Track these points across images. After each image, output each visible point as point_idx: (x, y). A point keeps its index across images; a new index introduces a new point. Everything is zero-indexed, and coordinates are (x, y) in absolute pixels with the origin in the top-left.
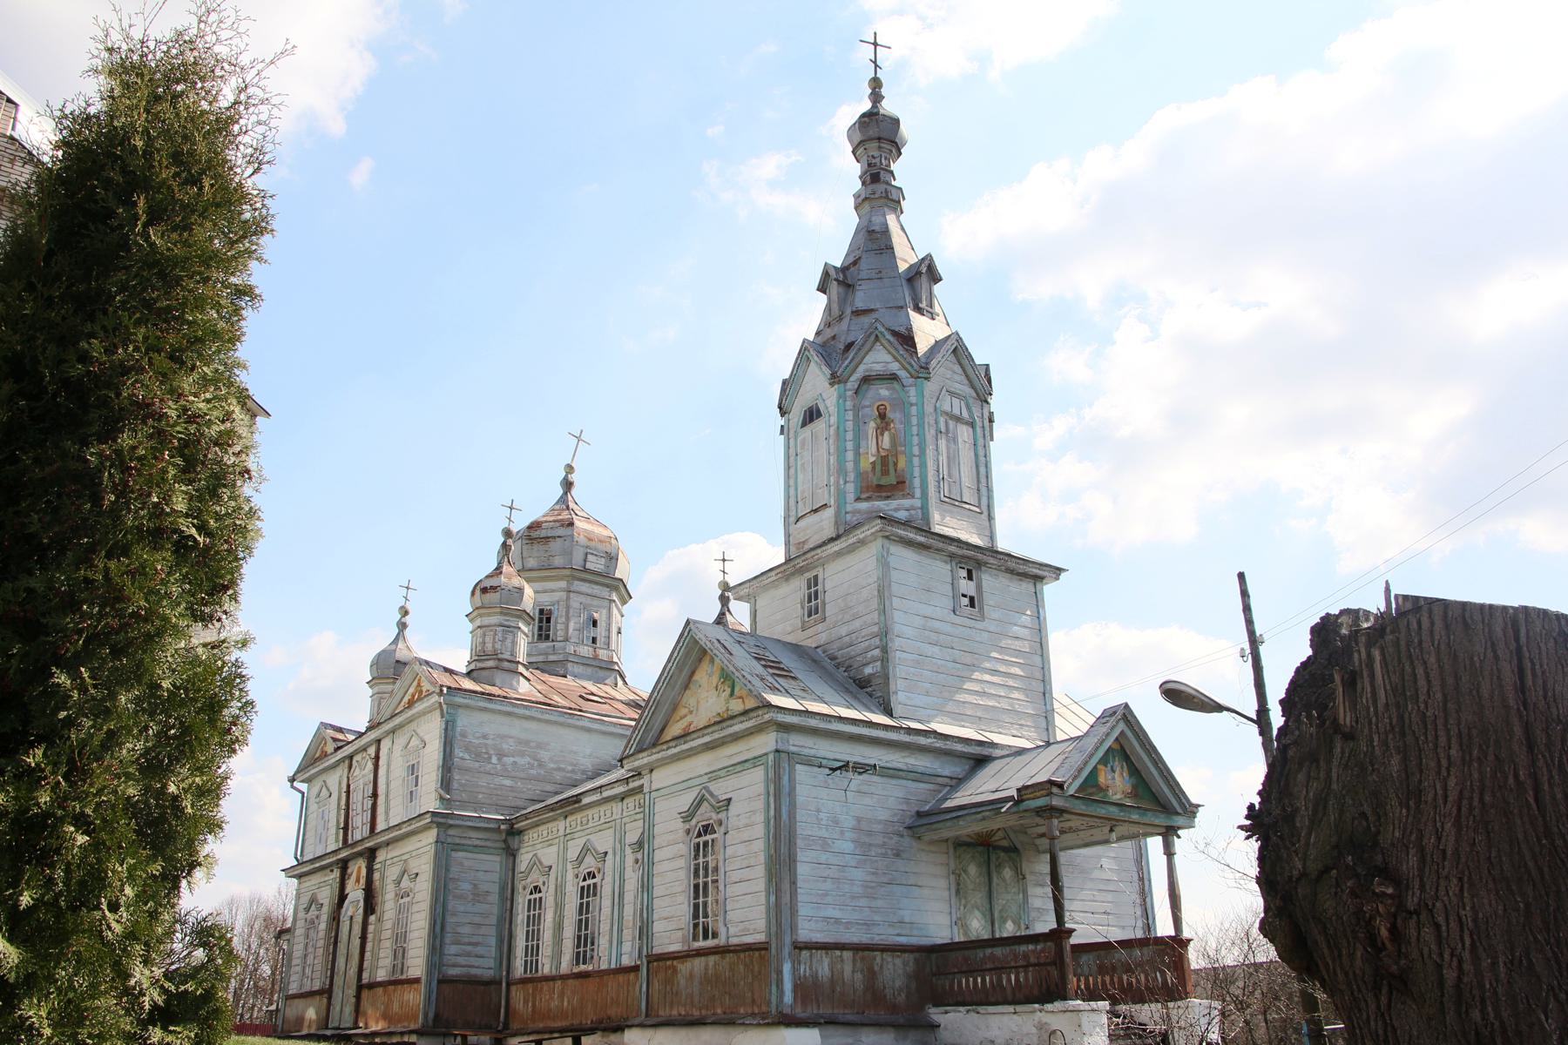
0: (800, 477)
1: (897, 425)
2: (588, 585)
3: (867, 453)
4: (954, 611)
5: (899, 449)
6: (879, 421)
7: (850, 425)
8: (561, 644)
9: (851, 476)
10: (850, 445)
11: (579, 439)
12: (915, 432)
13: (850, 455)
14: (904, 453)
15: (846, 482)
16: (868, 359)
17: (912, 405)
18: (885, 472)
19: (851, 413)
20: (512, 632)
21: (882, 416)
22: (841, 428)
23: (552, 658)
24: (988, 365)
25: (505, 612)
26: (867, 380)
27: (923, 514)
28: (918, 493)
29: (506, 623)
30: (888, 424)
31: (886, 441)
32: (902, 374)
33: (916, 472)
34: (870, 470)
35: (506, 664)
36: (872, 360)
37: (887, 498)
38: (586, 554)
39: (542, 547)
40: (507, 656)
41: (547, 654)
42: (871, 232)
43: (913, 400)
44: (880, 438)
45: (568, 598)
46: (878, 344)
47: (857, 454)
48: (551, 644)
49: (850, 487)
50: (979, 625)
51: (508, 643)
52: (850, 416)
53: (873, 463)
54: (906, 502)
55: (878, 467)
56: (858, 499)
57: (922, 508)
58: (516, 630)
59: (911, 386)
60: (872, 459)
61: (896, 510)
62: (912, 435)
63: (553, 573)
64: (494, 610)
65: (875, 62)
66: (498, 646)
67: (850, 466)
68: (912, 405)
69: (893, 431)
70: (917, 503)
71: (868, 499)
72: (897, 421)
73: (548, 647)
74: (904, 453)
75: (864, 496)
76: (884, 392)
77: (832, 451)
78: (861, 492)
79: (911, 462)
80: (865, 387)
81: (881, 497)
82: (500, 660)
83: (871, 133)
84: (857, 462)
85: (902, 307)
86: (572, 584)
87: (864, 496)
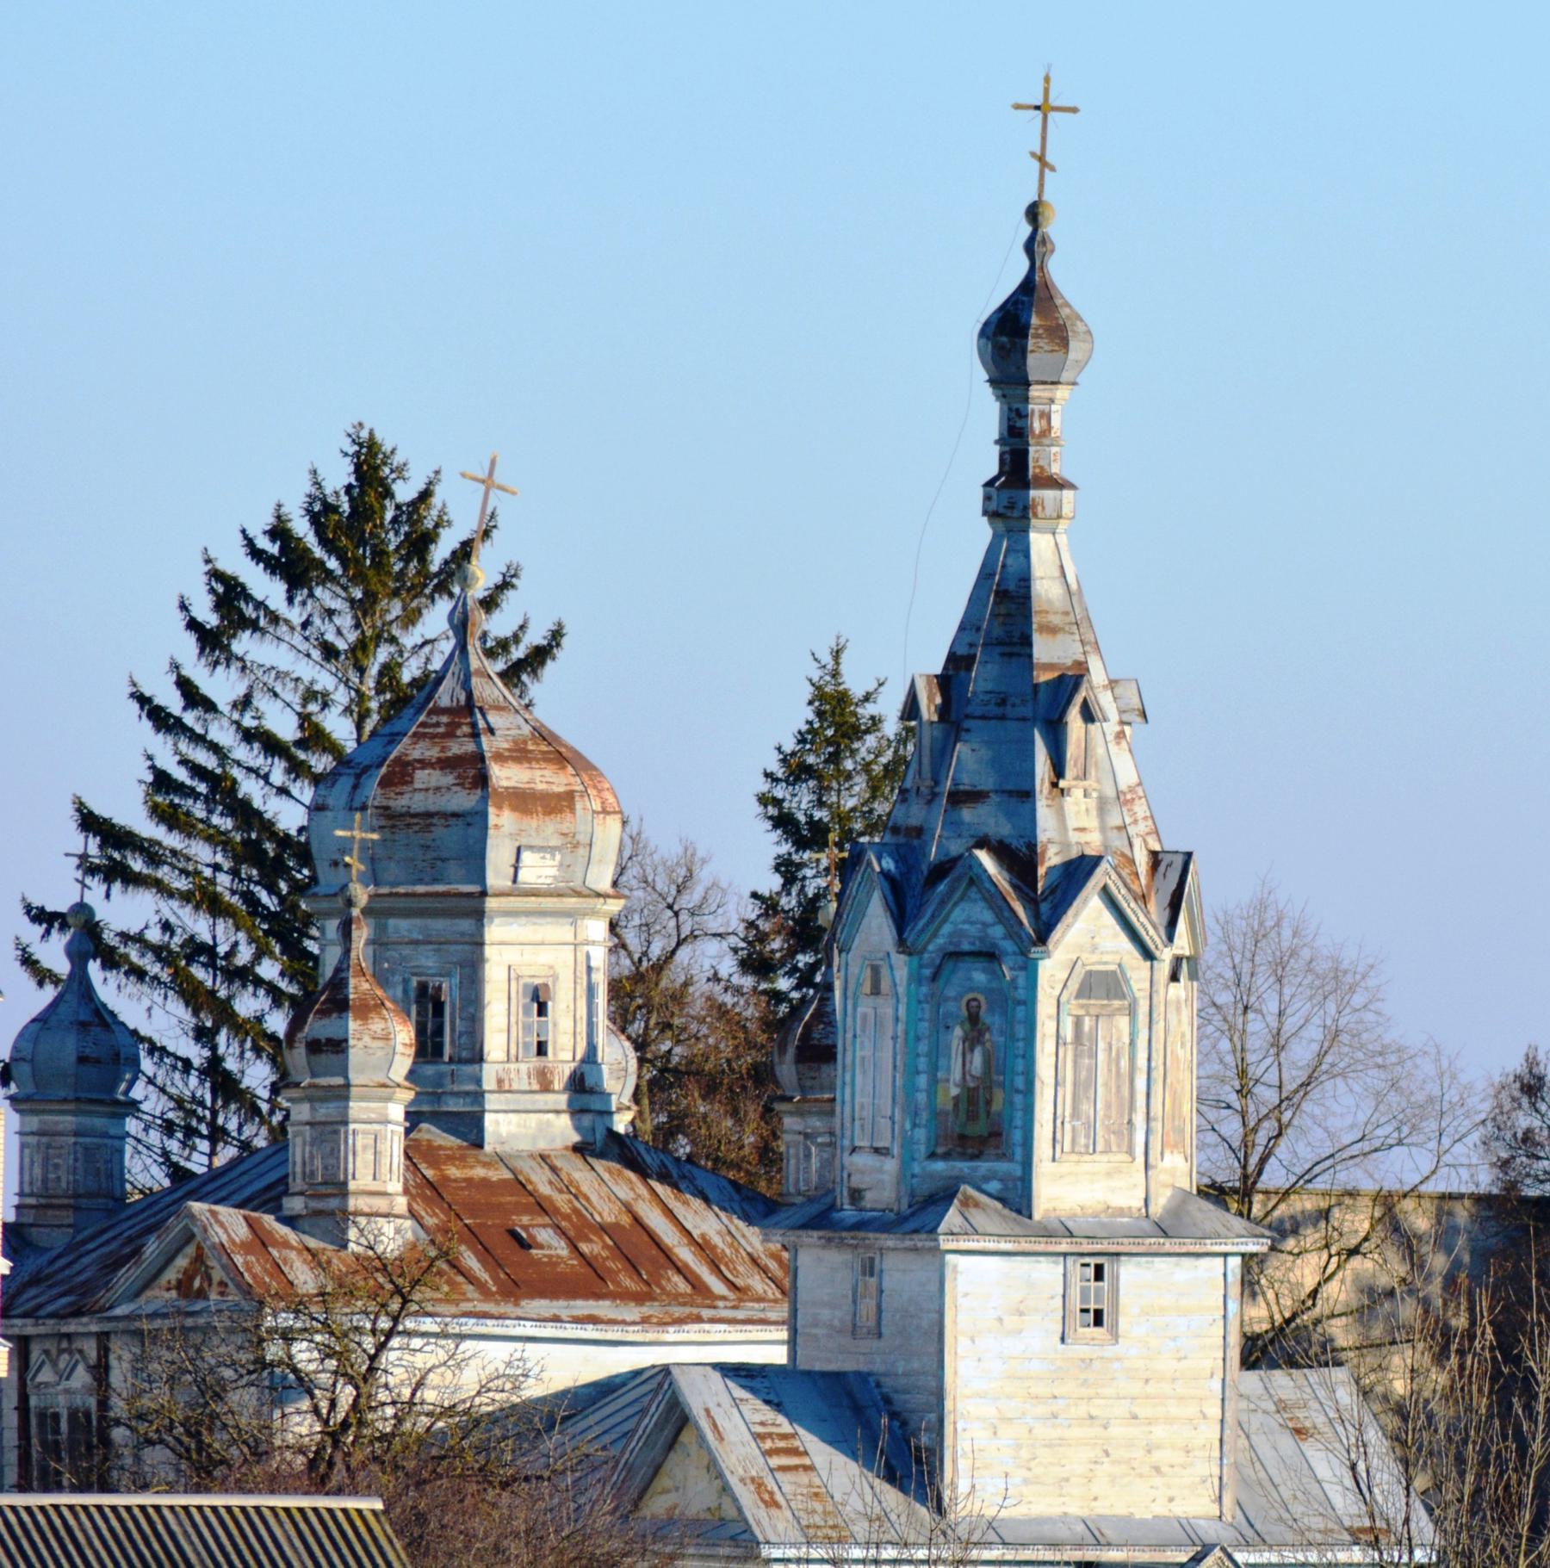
0: (859, 1079)
1: (994, 1038)
3: (948, 1081)
6: (967, 1026)
10: (922, 1063)
13: (922, 1081)
14: (1002, 1085)
15: (914, 1125)
18: (972, 1116)
21: (973, 1018)
26: (954, 956)
28: (1018, 1152)
30: (981, 1034)
34: (950, 1107)
37: (975, 1157)
42: (1002, 595)
44: (968, 1057)
46: (974, 889)
47: (934, 1081)
49: (921, 1134)
53: (957, 1099)
54: (1002, 1167)
55: (963, 1106)
56: (932, 1156)
60: (955, 1091)
65: (1041, 159)
67: (922, 1097)
69: (988, 1045)
71: (946, 1156)
76: (980, 977)
77: (898, 1063)
78: (937, 1145)
79: (1011, 1103)
80: (949, 965)
84: (932, 1092)
87: (940, 1150)
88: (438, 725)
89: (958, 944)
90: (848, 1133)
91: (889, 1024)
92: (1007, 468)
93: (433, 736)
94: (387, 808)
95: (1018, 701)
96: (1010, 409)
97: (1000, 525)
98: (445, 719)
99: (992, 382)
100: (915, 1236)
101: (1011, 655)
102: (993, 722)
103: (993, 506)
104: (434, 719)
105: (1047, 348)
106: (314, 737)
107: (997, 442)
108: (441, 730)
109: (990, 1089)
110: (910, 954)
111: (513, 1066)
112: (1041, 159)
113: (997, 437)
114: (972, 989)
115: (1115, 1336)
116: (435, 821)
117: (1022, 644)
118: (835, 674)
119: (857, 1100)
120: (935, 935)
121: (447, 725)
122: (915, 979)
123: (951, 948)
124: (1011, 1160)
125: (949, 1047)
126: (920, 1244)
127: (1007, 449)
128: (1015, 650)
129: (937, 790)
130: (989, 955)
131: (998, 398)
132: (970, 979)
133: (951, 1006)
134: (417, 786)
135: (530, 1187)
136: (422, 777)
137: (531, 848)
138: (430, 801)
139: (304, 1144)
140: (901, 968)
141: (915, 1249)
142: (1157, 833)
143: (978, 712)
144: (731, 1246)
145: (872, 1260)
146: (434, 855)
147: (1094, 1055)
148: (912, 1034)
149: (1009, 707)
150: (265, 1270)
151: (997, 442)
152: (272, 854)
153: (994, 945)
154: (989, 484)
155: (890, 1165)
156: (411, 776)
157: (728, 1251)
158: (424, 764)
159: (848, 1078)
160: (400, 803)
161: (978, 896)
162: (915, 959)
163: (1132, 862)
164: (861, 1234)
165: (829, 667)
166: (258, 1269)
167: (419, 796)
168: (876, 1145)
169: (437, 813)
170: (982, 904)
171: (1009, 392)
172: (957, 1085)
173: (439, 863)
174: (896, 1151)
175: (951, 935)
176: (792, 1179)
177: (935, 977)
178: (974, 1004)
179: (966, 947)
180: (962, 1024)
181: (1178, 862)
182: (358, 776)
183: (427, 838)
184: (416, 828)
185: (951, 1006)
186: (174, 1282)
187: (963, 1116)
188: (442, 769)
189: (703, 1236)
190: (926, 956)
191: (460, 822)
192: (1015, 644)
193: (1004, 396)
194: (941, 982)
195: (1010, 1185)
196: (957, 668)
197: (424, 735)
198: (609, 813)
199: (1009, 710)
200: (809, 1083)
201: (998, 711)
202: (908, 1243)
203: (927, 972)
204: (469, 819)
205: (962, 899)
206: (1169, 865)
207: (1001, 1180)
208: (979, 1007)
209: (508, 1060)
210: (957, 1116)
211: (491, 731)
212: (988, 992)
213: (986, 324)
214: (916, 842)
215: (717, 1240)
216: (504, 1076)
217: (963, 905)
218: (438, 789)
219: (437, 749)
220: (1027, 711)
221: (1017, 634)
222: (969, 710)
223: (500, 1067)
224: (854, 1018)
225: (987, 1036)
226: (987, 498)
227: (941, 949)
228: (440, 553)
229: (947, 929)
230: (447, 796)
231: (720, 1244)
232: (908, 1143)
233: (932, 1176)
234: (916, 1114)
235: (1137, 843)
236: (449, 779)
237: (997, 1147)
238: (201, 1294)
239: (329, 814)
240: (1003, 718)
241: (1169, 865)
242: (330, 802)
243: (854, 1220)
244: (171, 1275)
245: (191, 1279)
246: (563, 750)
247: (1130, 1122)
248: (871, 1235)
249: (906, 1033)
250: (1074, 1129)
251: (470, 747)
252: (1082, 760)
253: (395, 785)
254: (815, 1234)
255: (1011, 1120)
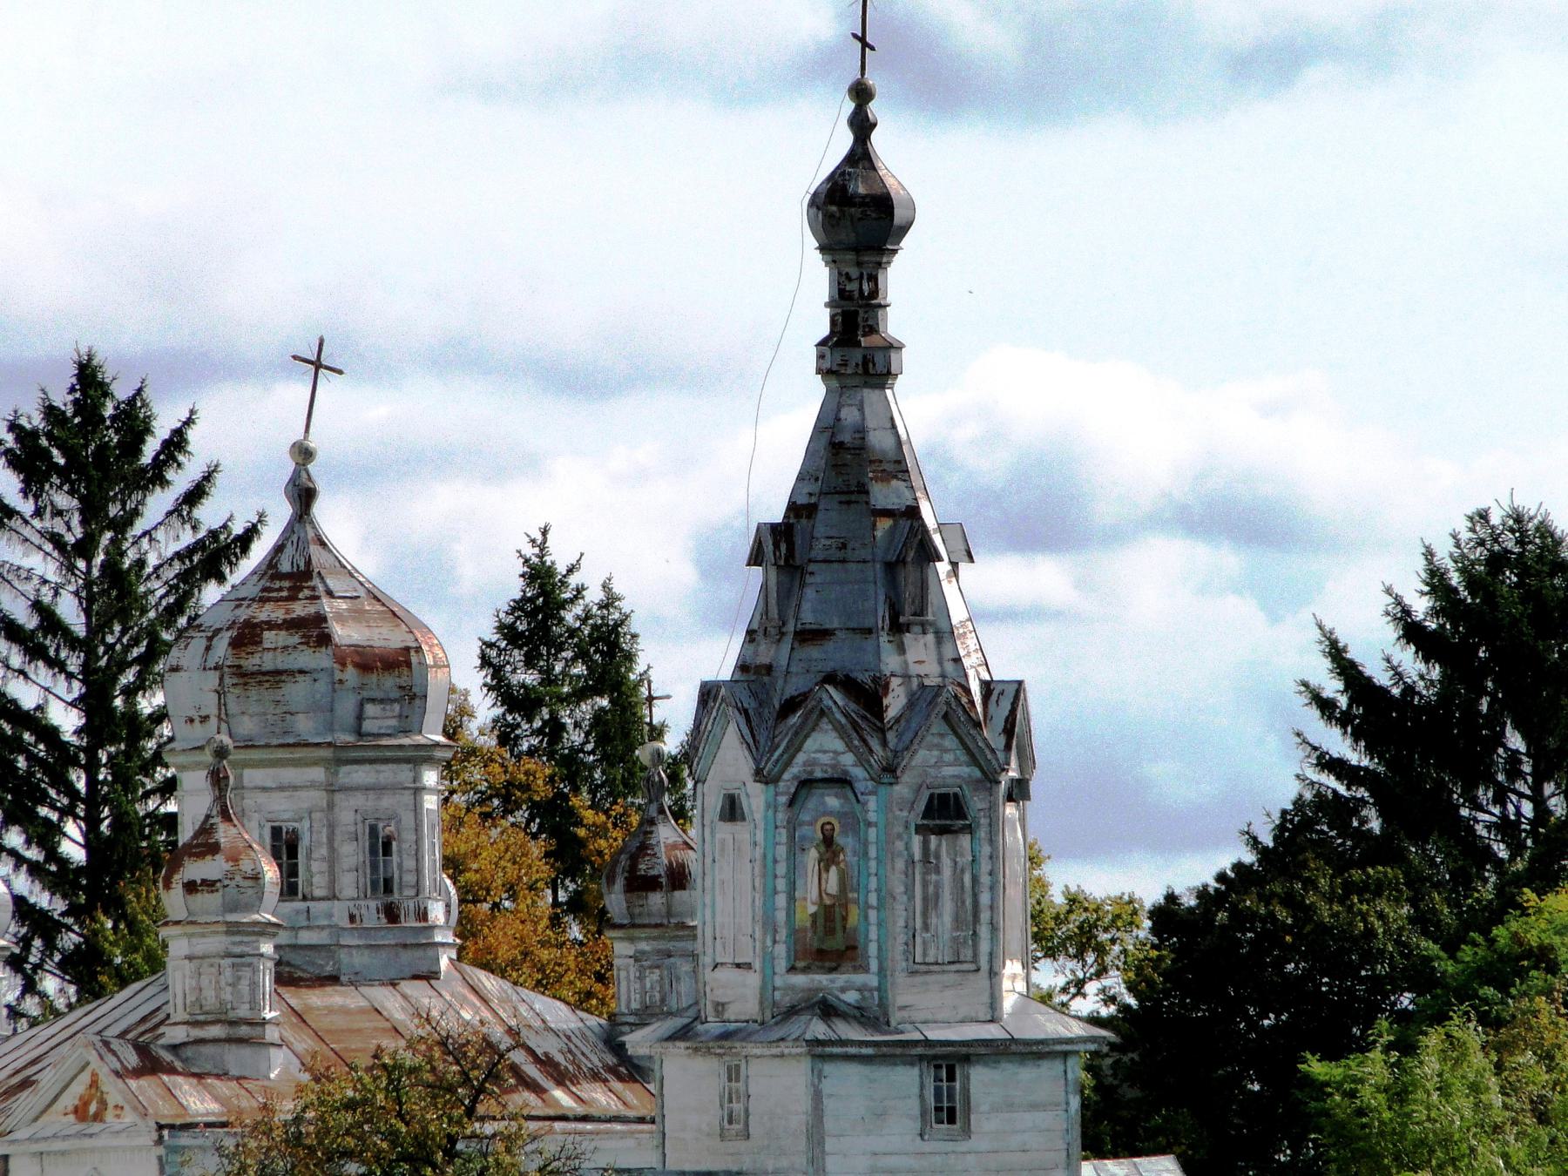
0: (719, 899)
1: (848, 857)
2: (367, 767)
3: (805, 899)
4: (921, 1135)
5: (850, 895)
6: (822, 849)
7: (782, 851)
8: (323, 905)
9: (782, 934)
10: (781, 884)
11: (318, 365)
12: (873, 870)
13: (781, 900)
14: (856, 902)
15: (775, 942)
16: (810, 744)
17: (869, 824)
18: (830, 931)
19: (784, 832)
20: (250, 965)
21: (828, 841)
22: (770, 857)
23: (306, 938)
24: (1020, 683)
25: (234, 929)
26: (807, 784)
27: (880, 999)
28: (874, 965)
29: (237, 950)
30: (835, 854)
31: (832, 882)
32: (858, 772)
33: (873, 935)
34: (808, 924)
35: (244, 1031)
36: (816, 747)
37: (832, 970)
38: (361, 705)
39: (269, 695)
40: (243, 1012)
41: (295, 929)
42: (836, 447)
43: (872, 817)
44: (824, 876)
45: (331, 806)
46: (825, 720)
47: (791, 898)
48: (302, 905)
49: (781, 950)
50: (963, 1146)
51: (244, 986)
52: (783, 836)
53: (814, 916)
54: (859, 979)
55: (821, 921)
56: (792, 969)
57: (879, 989)
58: (254, 960)
59: (871, 793)
60: (812, 909)
61: (843, 990)
62: (869, 875)
63: (299, 754)
64: (213, 928)
65: (862, 39)
66: (227, 995)
67: (781, 916)
68: (869, 824)
69: (842, 865)
70: (873, 980)
71: (806, 970)
72: (848, 851)
73: (298, 912)
74: (856, 902)
75: (800, 964)
76: (833, 802)
77: (757, 885)
78: (796, 959)
79: (866, 917)
80: (804, 792)
81: (822, 968)
82: (233, 1023)
83: (843, 236)
84: (791, 912)
85: (869, 631)
86: (336, 773)
87: (800, 964)
88: (281, 589)
89: (811, 773)
90: (709, 951)
91: (747, 848)
92: (839, 328)
93: (277, 600)
94: (239, 667)
95: (857, 545)
96: (840, 274)
97: (835, 384)
98: (286, 584)
99: (823, 249)
100: (781, 1043)
101: (849, 503)
102: (835, 566)
103: (827, 365)
104: (277, 584)
105: (874, 215)
106: (49, 620)
107: (827, 305)
108: (285, 594)
109: (845, 907)
110: (767, 783)
111: (362, 903)
112: (862, 39)
113: (827, 300)
114: (825, 814)
115: (967, 1132)
116: (283, 678)
117: (859, 492)
118: (542, 547)
119: (719, 920)
120: (788, 764)
121: (289, 589)
122: (772, 806)
123: (804, 776)
124: (866, 970)
125: (805, 868)
126: (786, 1051)
127: (839, 311)
128: (853, 498)
129: (784, 630)
130: (841, 781)
131: (827, 264)
132: (824, 804)
133: (806, 830)
134: (266, 646)
135: (385, 1013)
136: (269, 637)
137: (373, 700)
138: (280, 659)
139: (184, 976)
140: (756, 798)
141: (782, 1056)
142: (987, 665)
143: (820, 558)
144: (573, 1063)
145: (738, 1066)
146: (285, 709)
147: (938, 871)
148: (770, 857)
149: (849, 551)
150: (157, 1095)
151: (827, 305)
152: (10, 733)
153: (846, 772)
154: (822, 343)
155: (753, 980)
156: (260, 636)
157: (571, 1068)
158: (271, 625)
159: (708, 900)
160: (251, 662)
161: (830, 727)
162: (771, 787)
163: (968, 691)
164: (727, 1044)
165: (539, 542)
166: (151, 1093)
167: (268, 656)
168: (737, 961)
169: (286, 671)
170: (834, 734)
171: (837, 257)
172: (813, 904)
173: (288, 716)
174: (757, 965)
175: (805, 764)
176: (623, 998)
177: (791, 803)
178: (828, 827)
179: (818, 774)
180: (817, 847)
181: (1011, 691)
182: (210, 639)
183: (278, 695)
184: (267, 685)
185: (806, 830)
186: (71, 1108)
187: (820, 929)
188: (287, 629)
189: (546, 1054)
190: (781, 784)
191: (307, 678)
192: (852, 493)
193: (834, 261)
194: (796, 807)
195: (866, 994)
196: (798, 516)
197: (269, 600)
198: (440, 667)
199: (849, 554)
200: (637, 911)
201: (840, 555)
202: (775, 1051)
203: (783, 799)
204: (315, 676)
205: (813, 730)
206: (1002, 693)
207: (859, 990)
208: (833, 829)
209: (358, 898)
210: (815, 932)
211: (330, 594)
212: (841, 816)
213: (815, 195)
214: (766, 679)
215: (559, 1058)
216: (355, 912)
217: (814, 735)
218: (285, 648)
219: (283, 611)
220: (864, 554)
221: (853, 482)
222: (813, 554)
223: (351, 904)
224: (713, 842)
225: (842, 857)
226: (821, 357)
227: (795, 777)
228: (151, 447)
229: (801, 758)
230: (295, 655)
231: (563, 1062)
232: (769, 959)
233: (792, 988)
234: (775, 931)
235: (971, 673)
236: (296, 639)
237: (853, 959)
238: (98, 1117)
239: (182, 673)
240: (844, 561)
241: (1002, 693)
242: (184, 663)
243: (718, 1032)
244: (69, 1100)
245: (86, 1104)
246: (395, 609)
247: (975, 933)
248: (737, 1045)
249: (765, 856)
250: (924, 943)
251: (312, 610)
252: (919, 598)
253: (245, 645)
254: (682, 1045)
255: (867, 936)
